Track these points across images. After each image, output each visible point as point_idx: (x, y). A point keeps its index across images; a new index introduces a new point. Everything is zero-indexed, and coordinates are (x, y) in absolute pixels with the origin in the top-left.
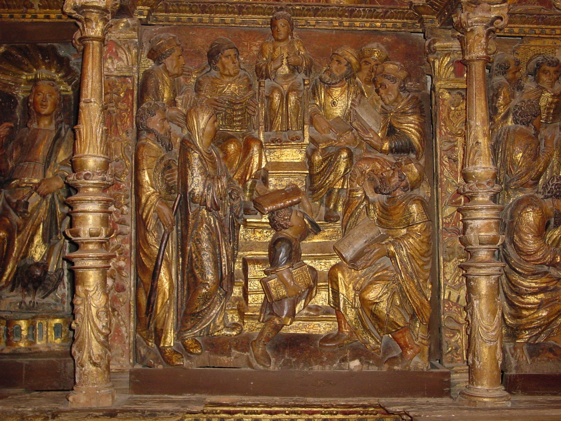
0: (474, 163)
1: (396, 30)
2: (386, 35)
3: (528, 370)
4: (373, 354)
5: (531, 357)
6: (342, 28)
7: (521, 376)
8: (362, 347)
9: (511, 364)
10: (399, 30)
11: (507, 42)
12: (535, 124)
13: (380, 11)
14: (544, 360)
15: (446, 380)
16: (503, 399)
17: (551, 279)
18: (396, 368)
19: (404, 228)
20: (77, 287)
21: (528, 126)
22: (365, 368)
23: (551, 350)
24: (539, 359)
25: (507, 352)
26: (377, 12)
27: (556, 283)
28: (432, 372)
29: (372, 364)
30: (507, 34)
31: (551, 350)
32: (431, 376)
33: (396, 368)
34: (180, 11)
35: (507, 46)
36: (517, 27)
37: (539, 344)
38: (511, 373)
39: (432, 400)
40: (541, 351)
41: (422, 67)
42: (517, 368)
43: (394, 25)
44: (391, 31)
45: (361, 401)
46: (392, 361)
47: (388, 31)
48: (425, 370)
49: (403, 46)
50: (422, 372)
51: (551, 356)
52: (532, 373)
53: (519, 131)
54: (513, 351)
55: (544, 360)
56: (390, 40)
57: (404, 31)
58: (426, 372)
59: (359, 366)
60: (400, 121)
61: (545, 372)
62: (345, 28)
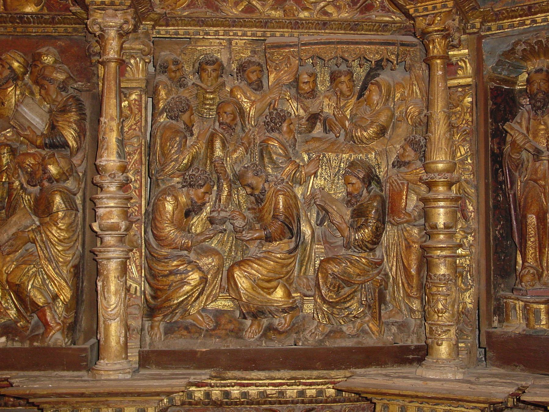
0: (101, 157)
1: (68, 34)
2: (60, 40)
3: (160, 346)
4: (21, 332)
5: (166, 334)
6: (16, 34)
7: (153, 352)
8: (13, 325)
9: (145, 340)
10: (70, 34)
11: (177, 44)
12: (184, 119)
13: (47, 17)
14: (177, 337)
15: (84, 355)
16: (119, 372)
17: (183, 263)
18: (36, 344)
19: (47, 216)
20: (72, 296)
21: (178, 121)
22: (10, 345)
23: (186, 328)
24: (172, 336)
25: (144, 330)
26: (45, 19)
27: (187, 266)
28: (71, 348)
29: (17, 341)
30: (173, 36)
31: (186, 328)
32: (70, 352)
33: (36, 344)
34: (512, 17)
35: (177, 47)
36: (182, 29)
37: (176, 322)
38: (145, 349)
39: (70, 373)
40: (176, 329)
41: (93, 68)
42: (150, 344)
43: (66, 30)
44: (63, 36)
45: (3, 375)
46: (33, 338)
47: (60, 35)
48: (64, 345)
49: (76, 49)
50: (61, 348)
51: (185, 333)
52: (164, 349)
53: (169, 126)
54: (150, 329)
55: (177, 337)
56: (63, 44)
57: (76, 35)
58: (64, 348)
59: (4, 342)
60: (58, 119)
61: (177, 348)
62: (19, 34)
